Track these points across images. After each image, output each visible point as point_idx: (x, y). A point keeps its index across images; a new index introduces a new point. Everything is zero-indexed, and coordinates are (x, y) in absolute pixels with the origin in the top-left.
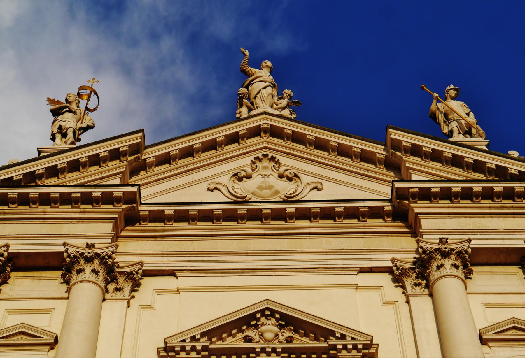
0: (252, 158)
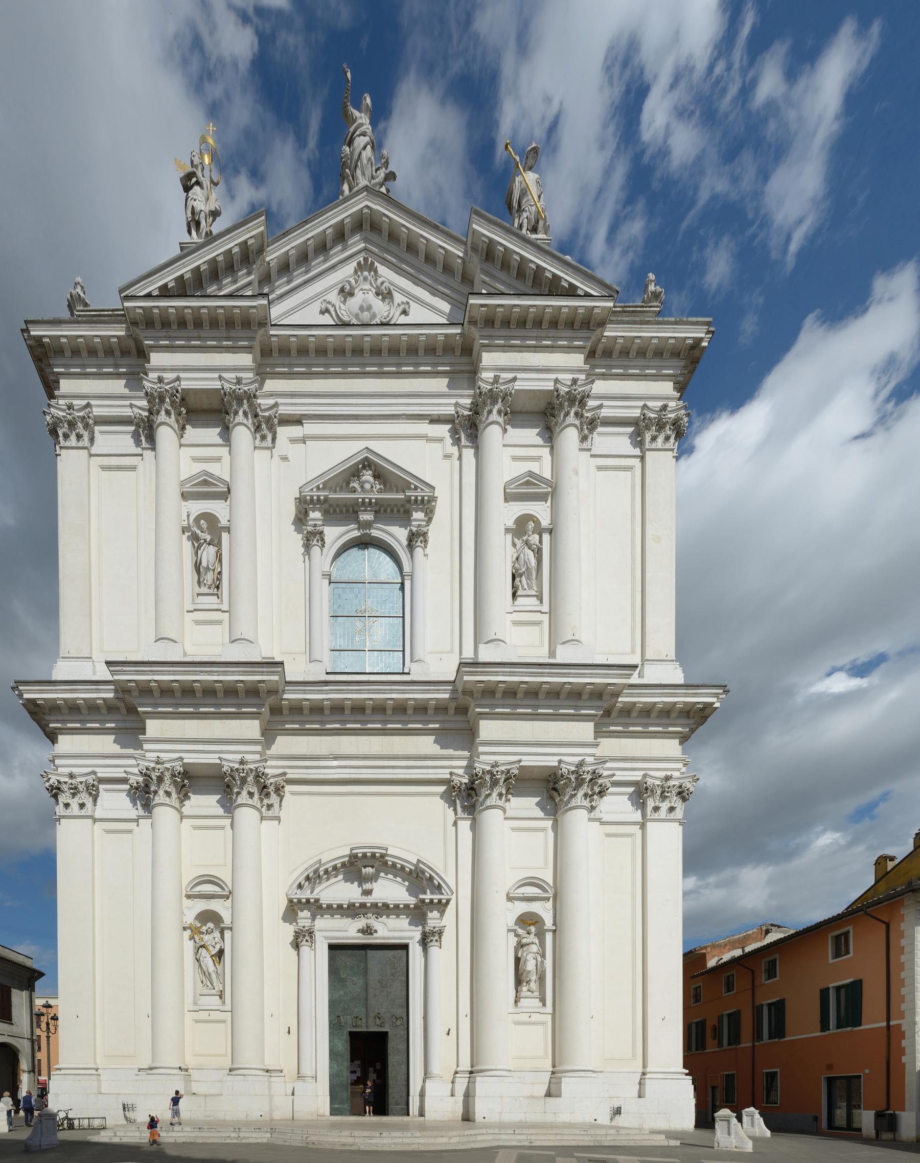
0: (354, 264)
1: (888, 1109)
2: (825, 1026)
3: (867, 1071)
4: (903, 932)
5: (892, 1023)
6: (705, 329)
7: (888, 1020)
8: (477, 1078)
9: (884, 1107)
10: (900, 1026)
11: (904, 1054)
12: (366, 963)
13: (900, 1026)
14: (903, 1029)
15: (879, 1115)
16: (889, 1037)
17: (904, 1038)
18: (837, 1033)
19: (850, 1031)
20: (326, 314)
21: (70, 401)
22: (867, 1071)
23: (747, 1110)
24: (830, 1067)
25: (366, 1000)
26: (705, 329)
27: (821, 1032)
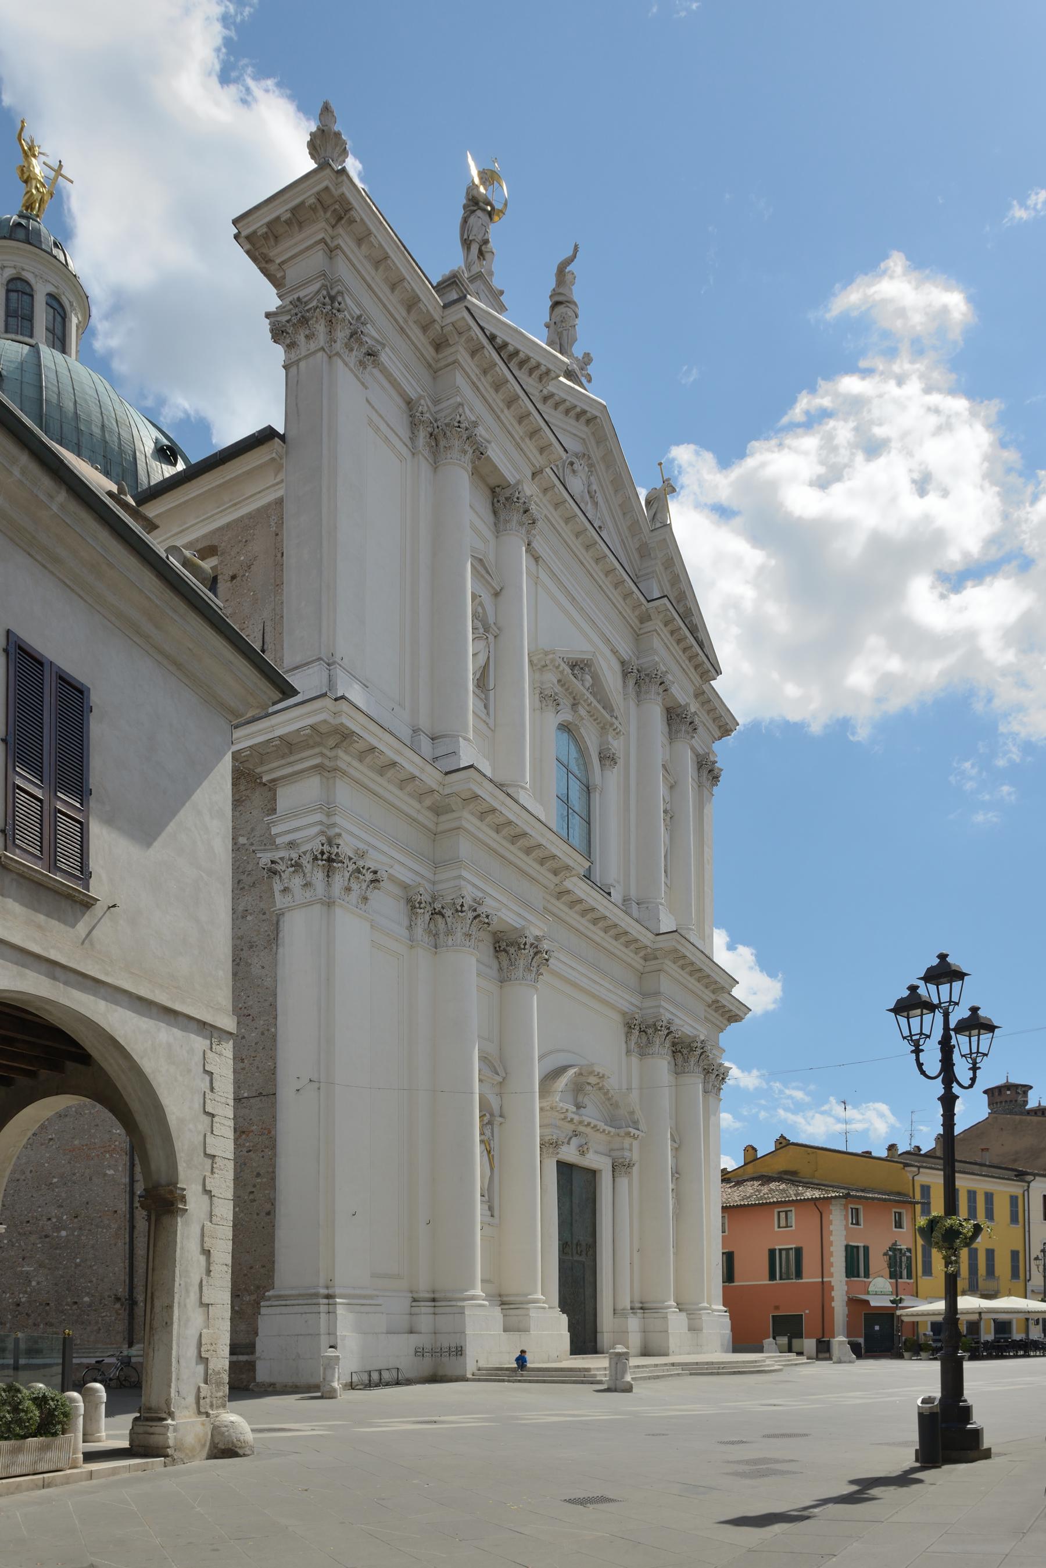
1: (823, 1337)
2: (772, 1277)
3: (807, 1312)
4: (831, 1221)
5: (825, 1280)
6: (416, 391)
7: (823, 1278)
8: (668, 1314)
9: (821, 1337)
10: (830, 1282)
11: (833, 1301)
12: (572, 1185)
13: (830, 1282)
14: (832, 1284)
15: (819, 1342)
16: (823, 1289)
17: (833, 1290)
18: (781, 1283)
19: (794, 1283)
20: (938, 960)
21: (296, 296)
22: (807, 1312)
23: (766, 1340)
24: (777, 1308)
25: (571, 1225)
26: (416, 391)
27: (770, 1280)
